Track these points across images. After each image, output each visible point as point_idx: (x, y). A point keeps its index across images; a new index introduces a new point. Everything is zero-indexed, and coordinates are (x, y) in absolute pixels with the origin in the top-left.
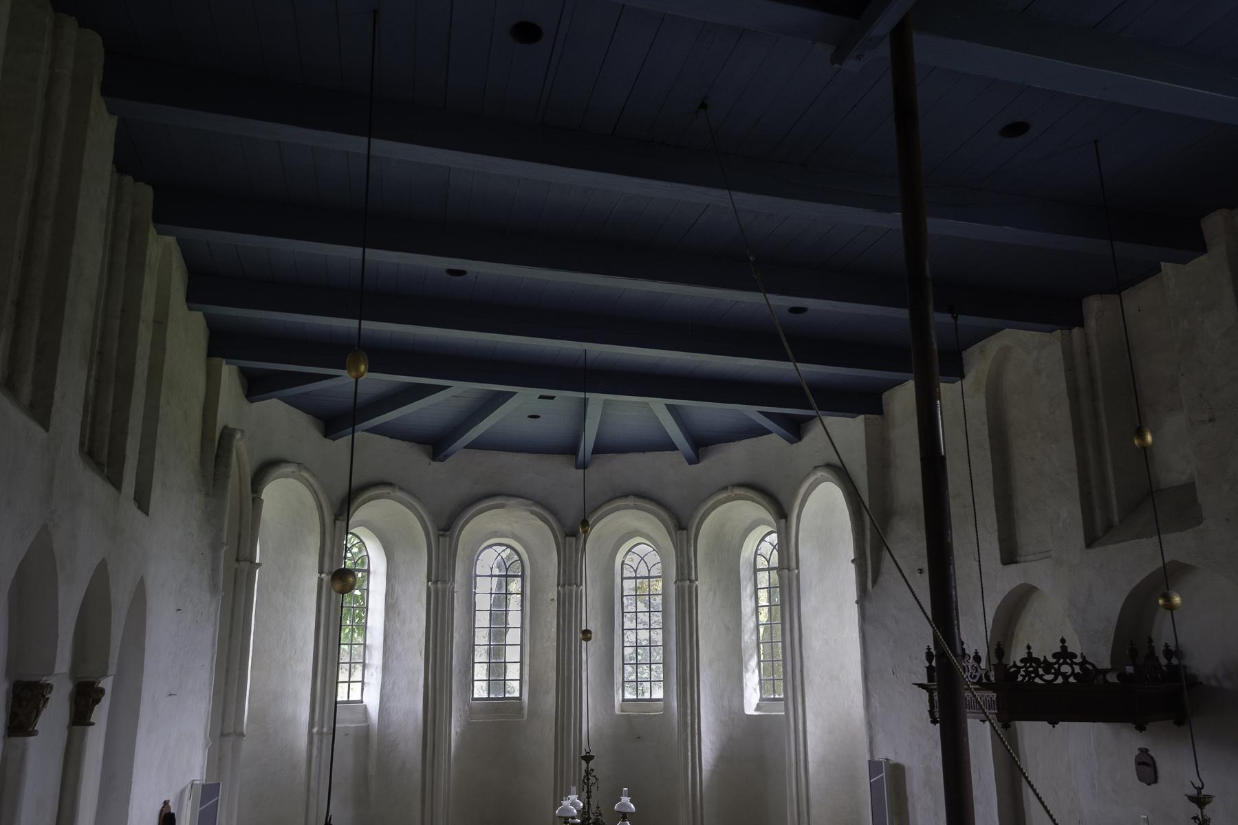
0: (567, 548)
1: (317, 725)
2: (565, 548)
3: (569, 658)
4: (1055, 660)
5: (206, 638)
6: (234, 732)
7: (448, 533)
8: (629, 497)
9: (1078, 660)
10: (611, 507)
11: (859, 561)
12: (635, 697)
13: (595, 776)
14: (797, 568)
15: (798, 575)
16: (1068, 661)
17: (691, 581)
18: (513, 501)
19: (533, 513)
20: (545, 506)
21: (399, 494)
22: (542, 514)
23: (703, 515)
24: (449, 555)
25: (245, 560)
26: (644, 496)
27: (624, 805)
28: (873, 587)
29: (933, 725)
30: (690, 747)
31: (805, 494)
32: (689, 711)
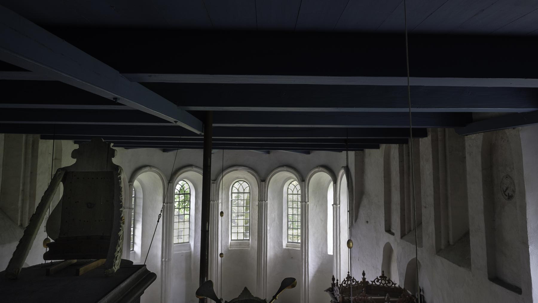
1: (164, 258)
2: (260, 186)
4: (380, 278)
7: (215, 182)
9: (387, 279)
10: (277, 170)
12: (292, 241)
14: (340, 204)
15: (340, 207)
16: (384, 279)
17: (306, 202)
18: (240, 168)
19: (248, 172)
20: (253, 169)
21: (195, 169)
24: (216, 190)
25: (127, 208)
28: (355, 223)
30: (304, 267)
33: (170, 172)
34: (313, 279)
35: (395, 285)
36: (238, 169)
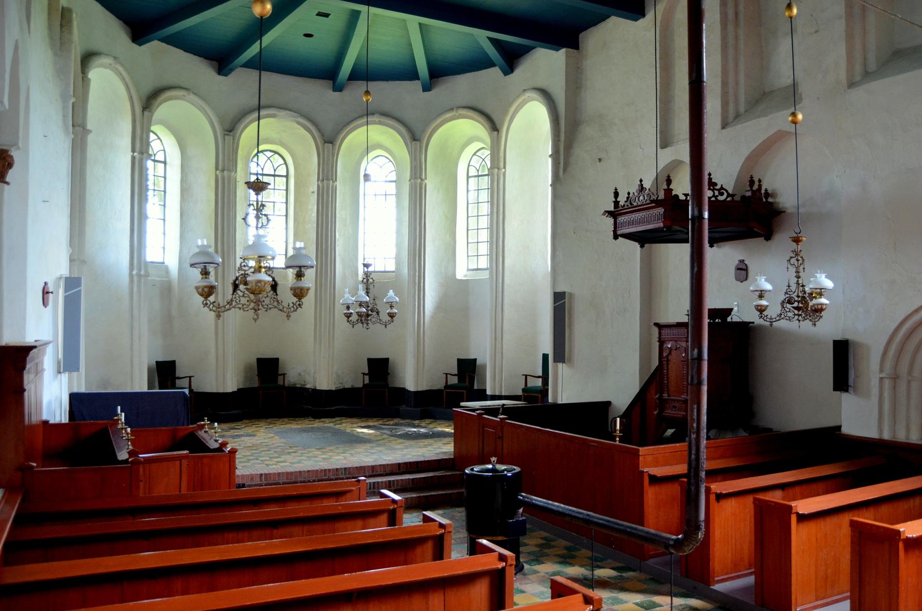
0: (326, 152)
2: (324, 152)
3: (327, 235)
5: (63, 165)
6: (78, 259)
7: (231, 133)
8: (375, 115)
9: (718, 187)
11: (555, 156)
13: (372, 278)
14: (505, 168)
15: (504, 174)
16: (712, 188)
17: (422, 180)
18: (283, 113)
19: (299, 123)
21: (192, 97)
22: (305, 124)
23: (433, 130)
26: (388, 115)
27: (391, 297)
29: (614, 240)
31: (514, 112)
32: (417, 274)
33: (147, 88)
34: (434, 316)
35: (733, 198)
36: (277, 113)
